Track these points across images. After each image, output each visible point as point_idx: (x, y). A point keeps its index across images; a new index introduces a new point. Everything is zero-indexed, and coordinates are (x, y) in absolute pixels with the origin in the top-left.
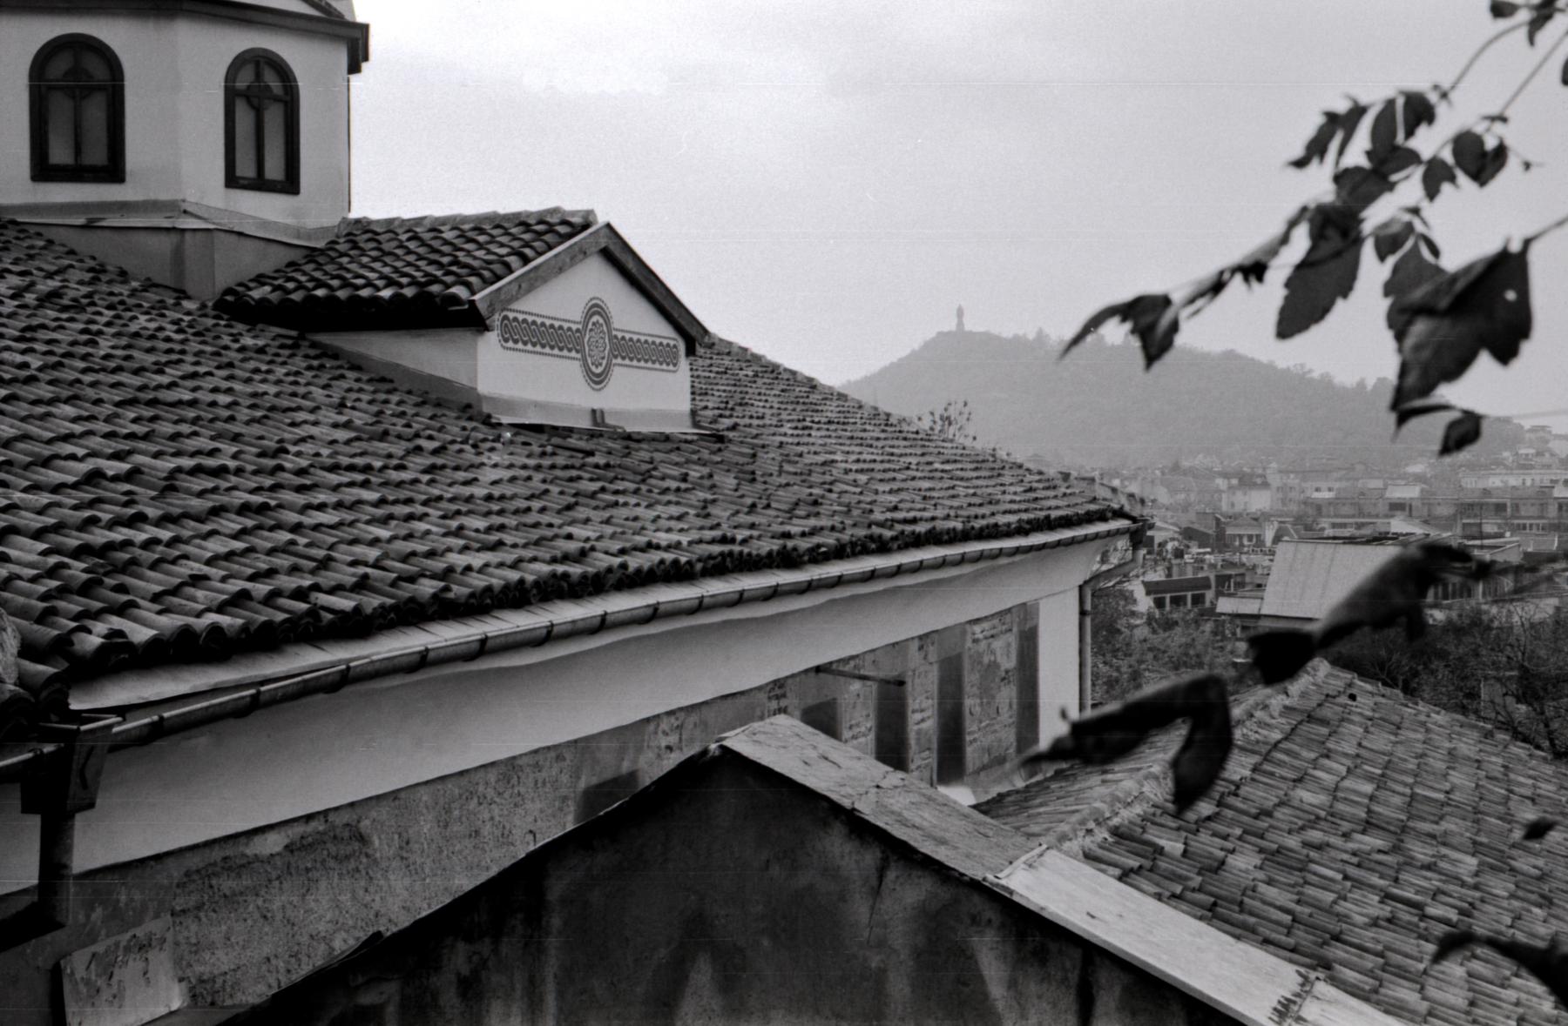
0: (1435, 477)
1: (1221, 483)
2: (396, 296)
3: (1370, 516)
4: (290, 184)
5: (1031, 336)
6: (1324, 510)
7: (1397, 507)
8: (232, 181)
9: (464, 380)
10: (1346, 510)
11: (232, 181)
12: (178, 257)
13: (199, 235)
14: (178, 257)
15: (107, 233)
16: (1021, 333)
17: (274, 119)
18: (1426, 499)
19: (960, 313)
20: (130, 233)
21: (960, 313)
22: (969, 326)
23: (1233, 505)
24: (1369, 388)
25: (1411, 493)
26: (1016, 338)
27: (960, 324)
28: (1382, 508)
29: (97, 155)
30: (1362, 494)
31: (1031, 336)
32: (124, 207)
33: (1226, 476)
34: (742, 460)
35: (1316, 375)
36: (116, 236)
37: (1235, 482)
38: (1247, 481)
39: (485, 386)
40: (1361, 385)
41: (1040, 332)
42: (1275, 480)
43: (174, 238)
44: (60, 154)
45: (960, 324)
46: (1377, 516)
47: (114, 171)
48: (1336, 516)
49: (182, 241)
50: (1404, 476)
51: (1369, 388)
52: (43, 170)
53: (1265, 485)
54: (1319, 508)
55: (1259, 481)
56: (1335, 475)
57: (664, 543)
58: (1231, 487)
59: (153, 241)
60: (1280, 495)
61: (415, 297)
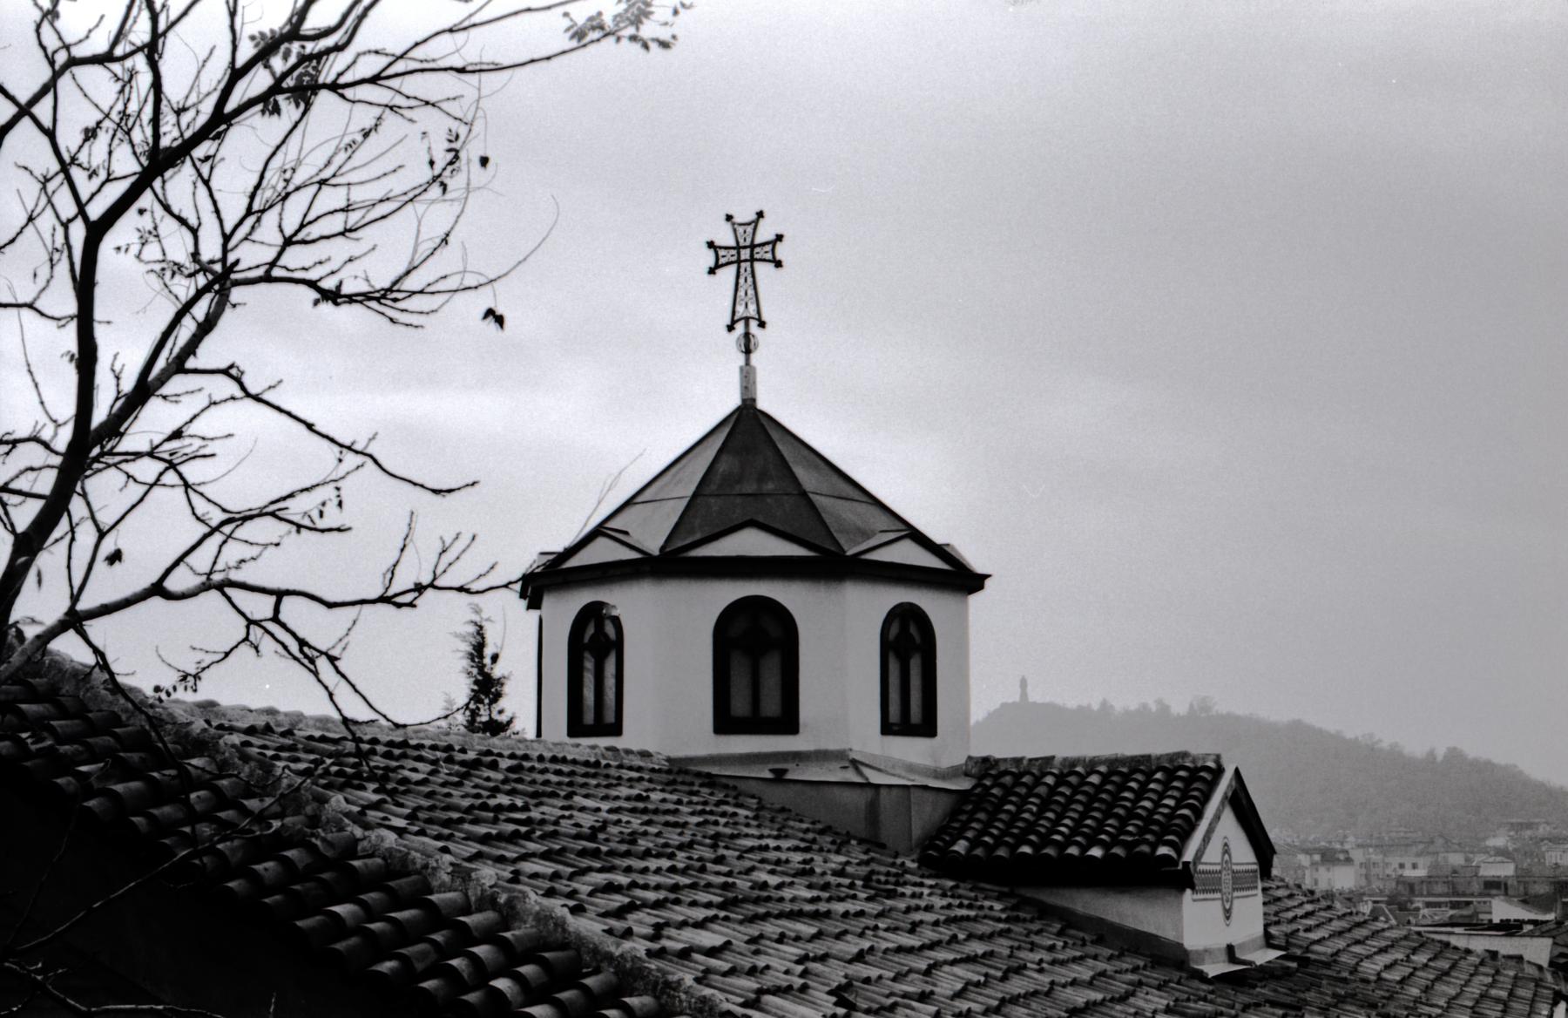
0: (1516, 850)
1: (1304, 859)
2: (1108, 857)
3: (1464, 895)
4: (927, 728)
5: (1095, 707)
6: (1417, 888)
7: (1494, 886)
8: (887, 729)
9: (1168, 933)
10: (1439, 889)
11: (887, 729)
12: (873, 809)
13: (895, 792)
14: (873, 809)
15: (798, 787)
16: (1085, 703)
17: (915, 665)
18: (1523, 877)
19: (1023, 683)
20: (826, 789)
21: (1023, 683)
22: (1035, 696)
23: (1316, 882)
24: (1440, 758)
25: (1506, 870)
26: (1080, 709)
27: (1024, 694)
28: (1476, 887)
29: (771, 706)
30: (1455, 872)
31: (1095, 707)
32: (798, 757)
33: (1307, 852)
34: (791, 823)
35: (1385, 745)
36: (808, 790)
37: (1317, 857)
38: (1329, 857)
39: (1191, 942)
40: (1432, 754)
41: (1104, 704)
42: (1357, 855)
43: (869, 793)
44: (740, 706)
45: (1024, 694)
46: (1472, 895)
47: (788, 722)
48: (1429, 895)
49: (878, 794)
50: (1486, 851)
51: (1440, 758)
52: (725, 723)
53: (1349, 861)
54: (1411, 886)
55: (1342, 857)
56: (1414, 849)
57: (653, 884)
58: (1313, 864)
59: (848, 796)
60: (1364, 871)
61: (1104, 857)
